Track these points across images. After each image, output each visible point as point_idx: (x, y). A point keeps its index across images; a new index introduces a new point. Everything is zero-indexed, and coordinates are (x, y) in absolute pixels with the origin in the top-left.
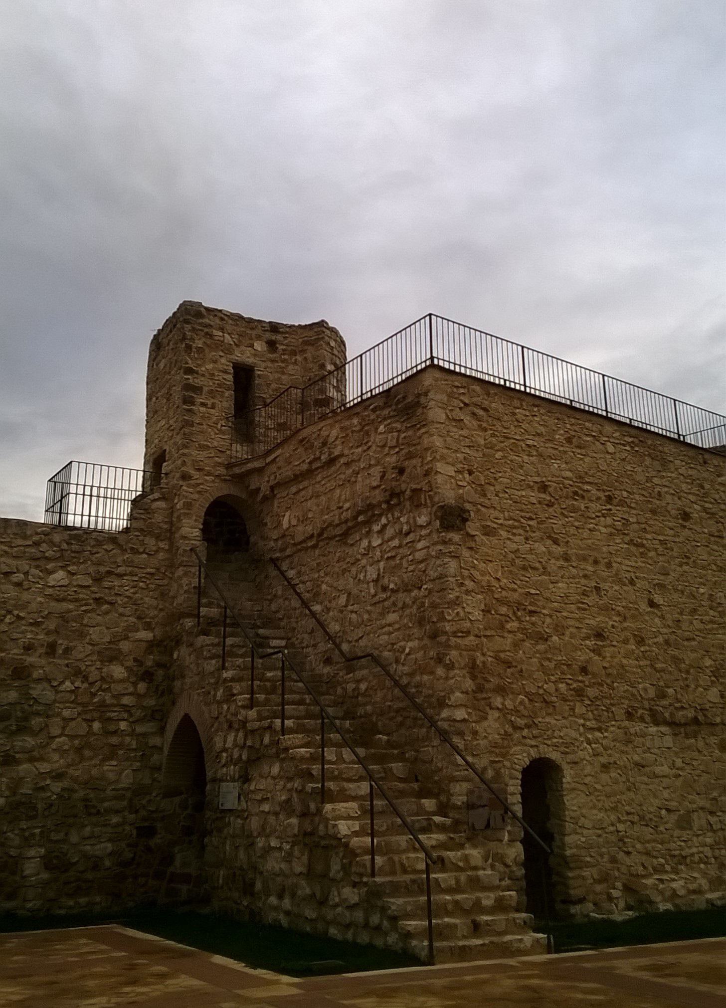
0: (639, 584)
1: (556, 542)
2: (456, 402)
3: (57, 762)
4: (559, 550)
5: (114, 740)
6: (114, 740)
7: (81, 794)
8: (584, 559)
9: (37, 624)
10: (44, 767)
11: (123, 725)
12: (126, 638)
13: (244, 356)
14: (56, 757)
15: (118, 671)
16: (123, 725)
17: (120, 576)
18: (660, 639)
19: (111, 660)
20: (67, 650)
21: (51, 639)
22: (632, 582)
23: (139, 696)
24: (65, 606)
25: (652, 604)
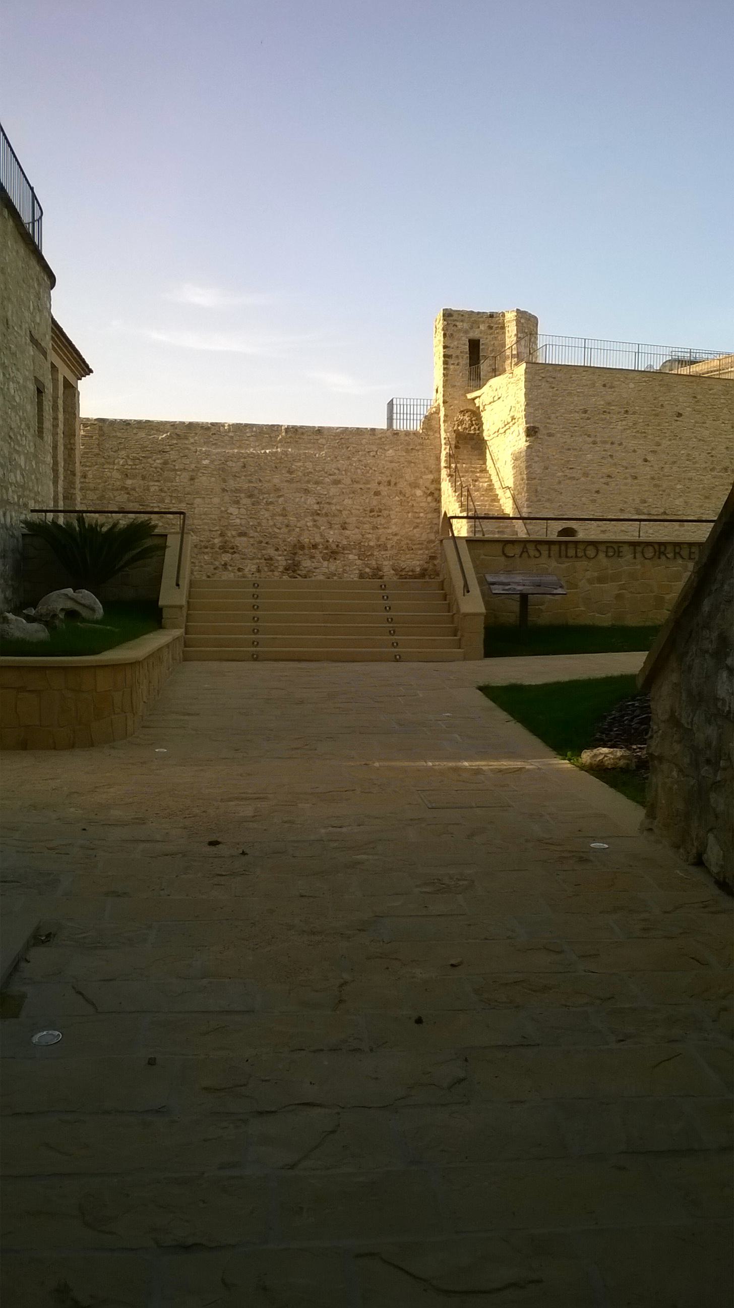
0: (639, 451)
1: (589, 436)
2: (537, 377)
3: (394, 529)
4: (590, 440)
5: (418, 521)
6: (418, 521)
7: (405, 542)
8: (605, 442)
9: (382, 473)
10: (389, 531)
11: (422, 515)
12: (421, 477)
13: (475, 334)
14: (394, 527)
15: (419, 493)
16: (422, 515)
17: (418, 450)
18: (649, 477)
19: (415, 487)
20: (395, 484)
21: (388, 479)
22: (634, 451)
23: (429, 503)
24: (393, 464)
25: (646, 460)
